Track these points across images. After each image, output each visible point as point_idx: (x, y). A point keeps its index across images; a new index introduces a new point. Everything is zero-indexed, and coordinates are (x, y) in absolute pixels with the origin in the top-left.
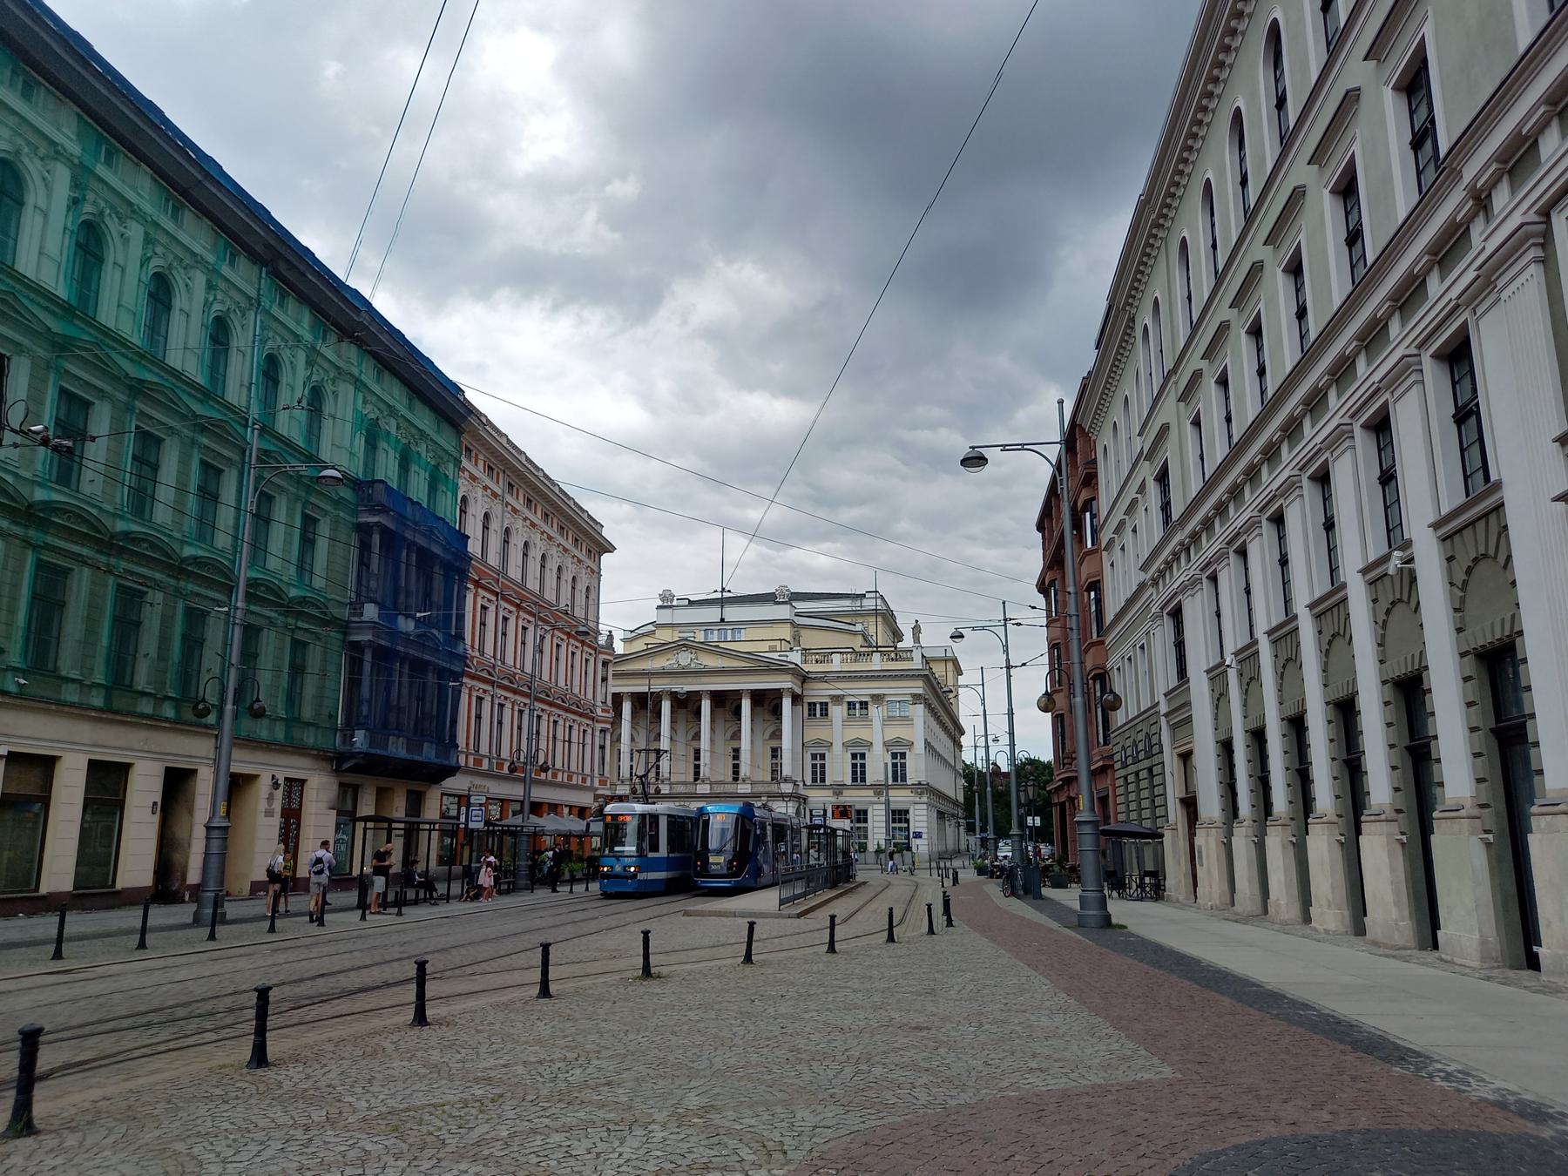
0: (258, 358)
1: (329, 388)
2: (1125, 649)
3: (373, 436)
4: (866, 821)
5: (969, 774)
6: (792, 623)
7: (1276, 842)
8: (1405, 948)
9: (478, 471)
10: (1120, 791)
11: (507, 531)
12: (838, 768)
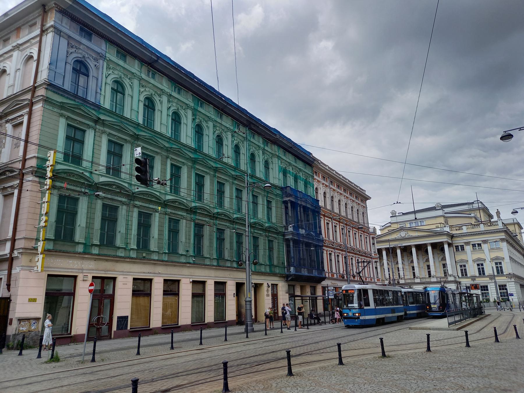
1: (270, 161)
3: (285, 173)
4: (487, 290)
6: (444, 217)
11: (332, 197)
12: (472, 270)
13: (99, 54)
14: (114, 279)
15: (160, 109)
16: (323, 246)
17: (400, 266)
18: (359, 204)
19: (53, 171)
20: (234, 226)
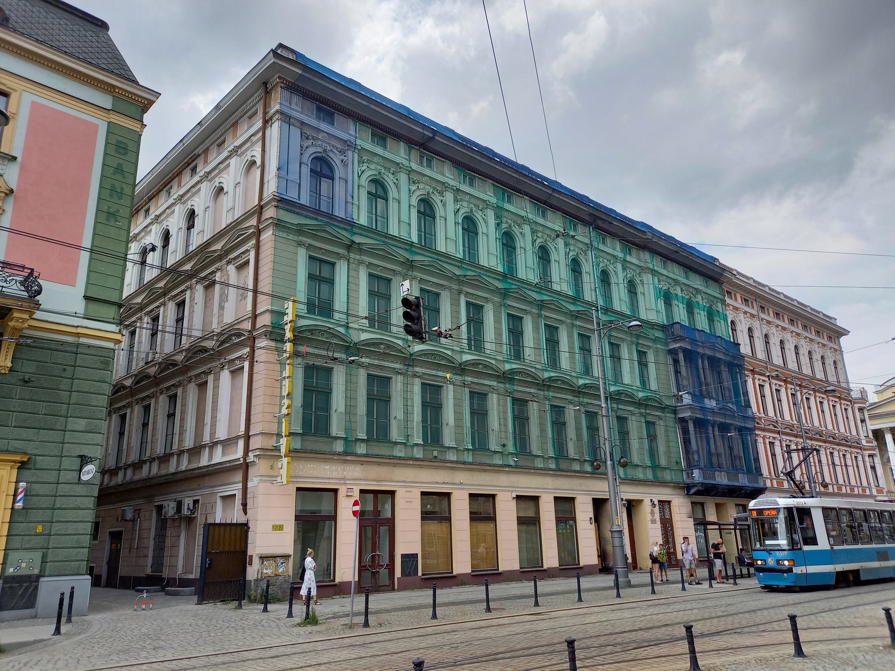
0: (597, 273)
1: (638, 279)
3: (668, 299)
9: (739, 304)
11: (766, 336)
13: (346, 142)
14: (392, 493)
15: (343, 176)
19: (294, 330)
20: (546, 393)
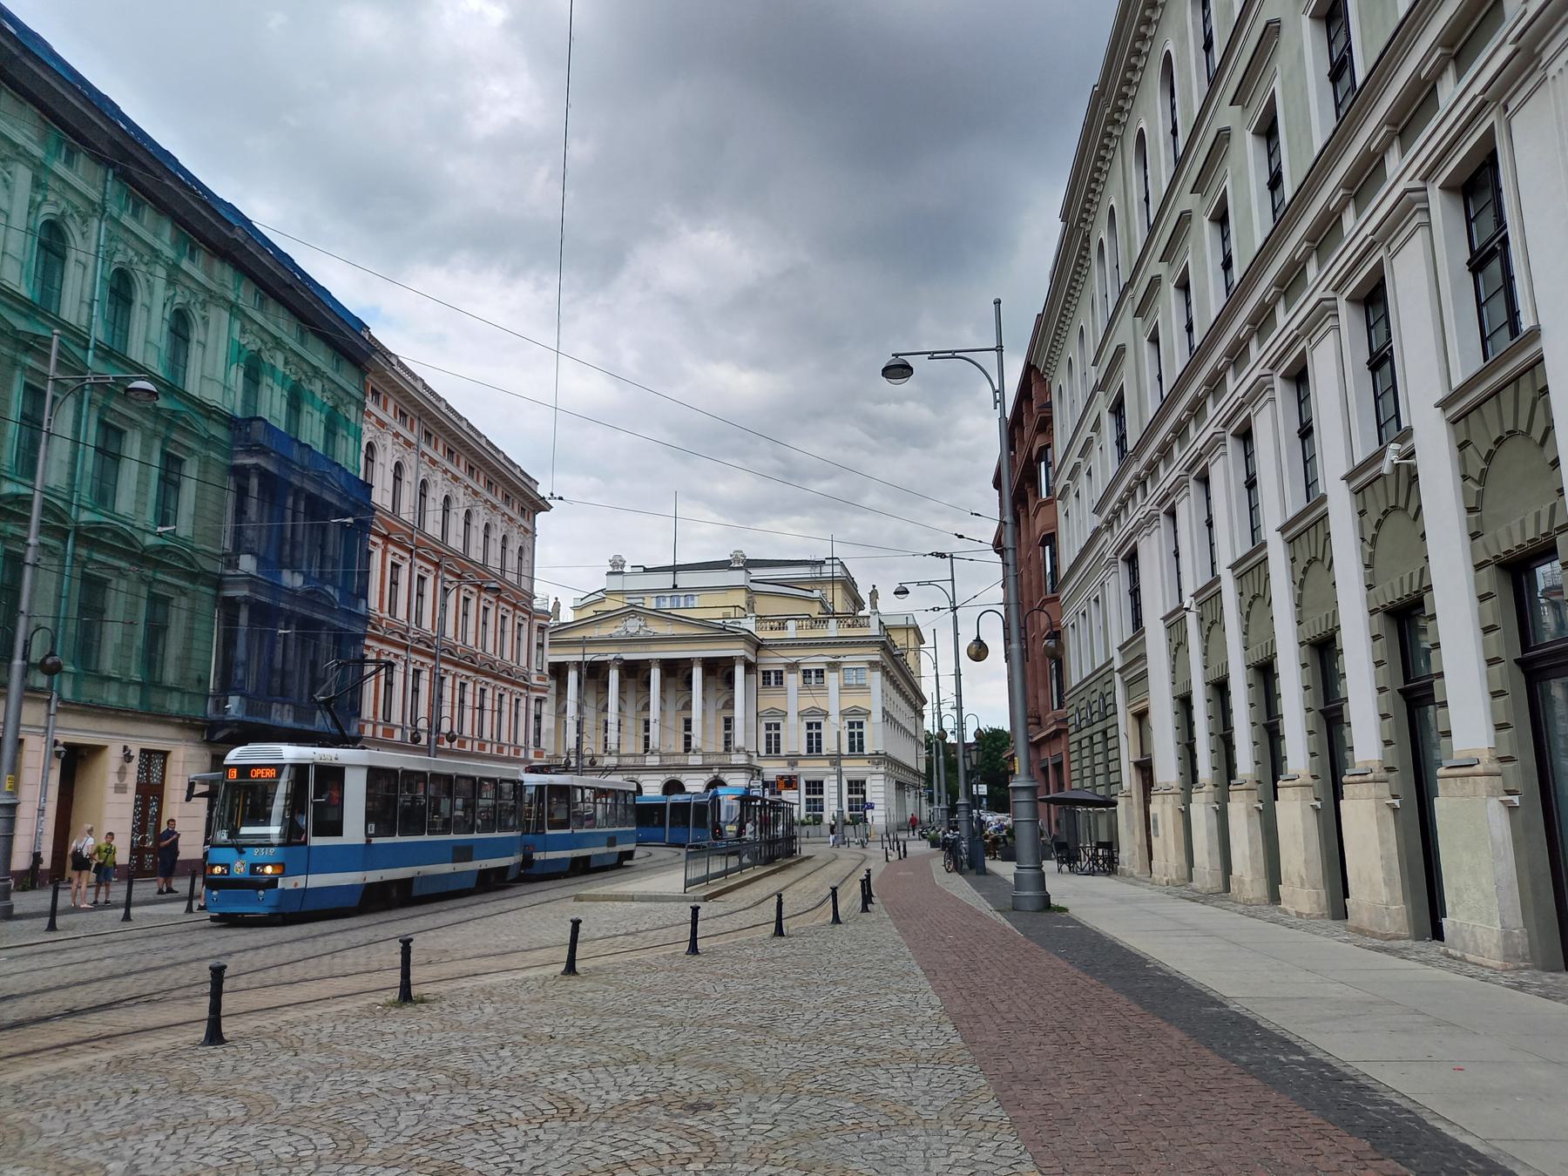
0: (103, 271)
1: (196, 313)
2: (1080, 603)
3: (254, 371)
4: (821, 792)
5: (935, 743)
6: (747, 589)
7: (1240, 809)
8: (1398, 938)
9: (388, 416)
10: (1074, 757)
11: (424, 484)
12: (794, 739)
16: (364, 637)
17: (612, 716)
18: (511, 519)
